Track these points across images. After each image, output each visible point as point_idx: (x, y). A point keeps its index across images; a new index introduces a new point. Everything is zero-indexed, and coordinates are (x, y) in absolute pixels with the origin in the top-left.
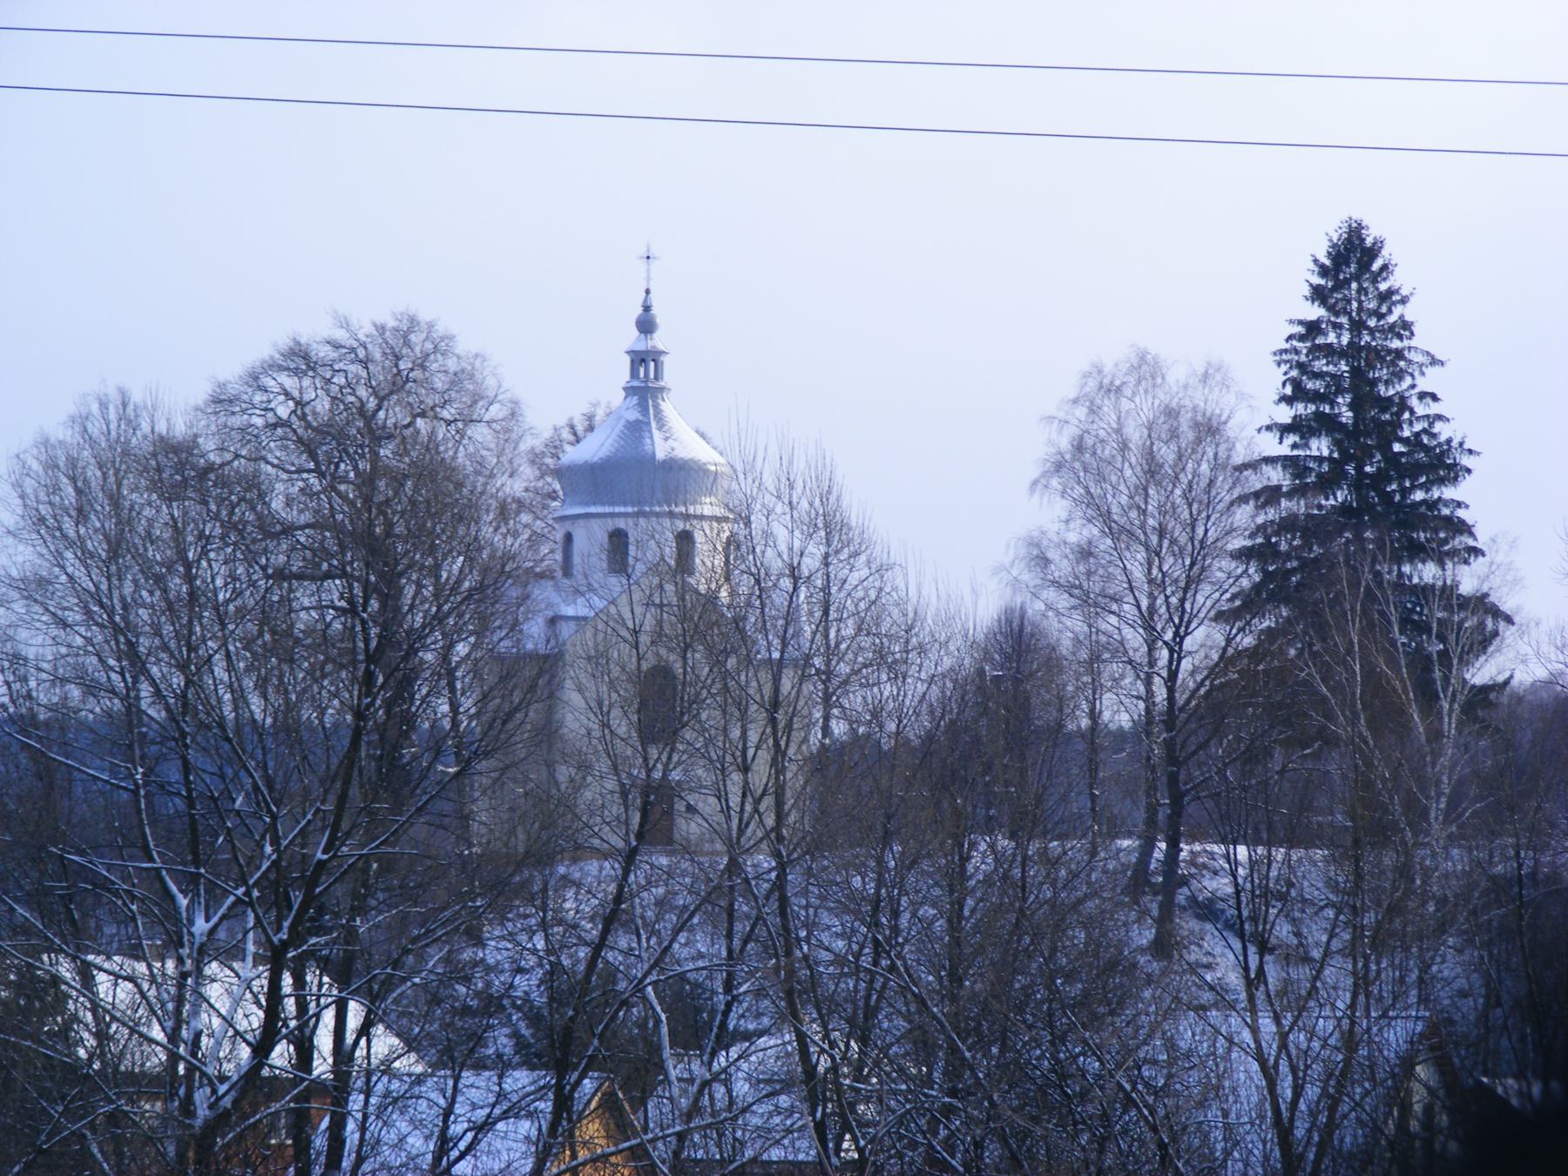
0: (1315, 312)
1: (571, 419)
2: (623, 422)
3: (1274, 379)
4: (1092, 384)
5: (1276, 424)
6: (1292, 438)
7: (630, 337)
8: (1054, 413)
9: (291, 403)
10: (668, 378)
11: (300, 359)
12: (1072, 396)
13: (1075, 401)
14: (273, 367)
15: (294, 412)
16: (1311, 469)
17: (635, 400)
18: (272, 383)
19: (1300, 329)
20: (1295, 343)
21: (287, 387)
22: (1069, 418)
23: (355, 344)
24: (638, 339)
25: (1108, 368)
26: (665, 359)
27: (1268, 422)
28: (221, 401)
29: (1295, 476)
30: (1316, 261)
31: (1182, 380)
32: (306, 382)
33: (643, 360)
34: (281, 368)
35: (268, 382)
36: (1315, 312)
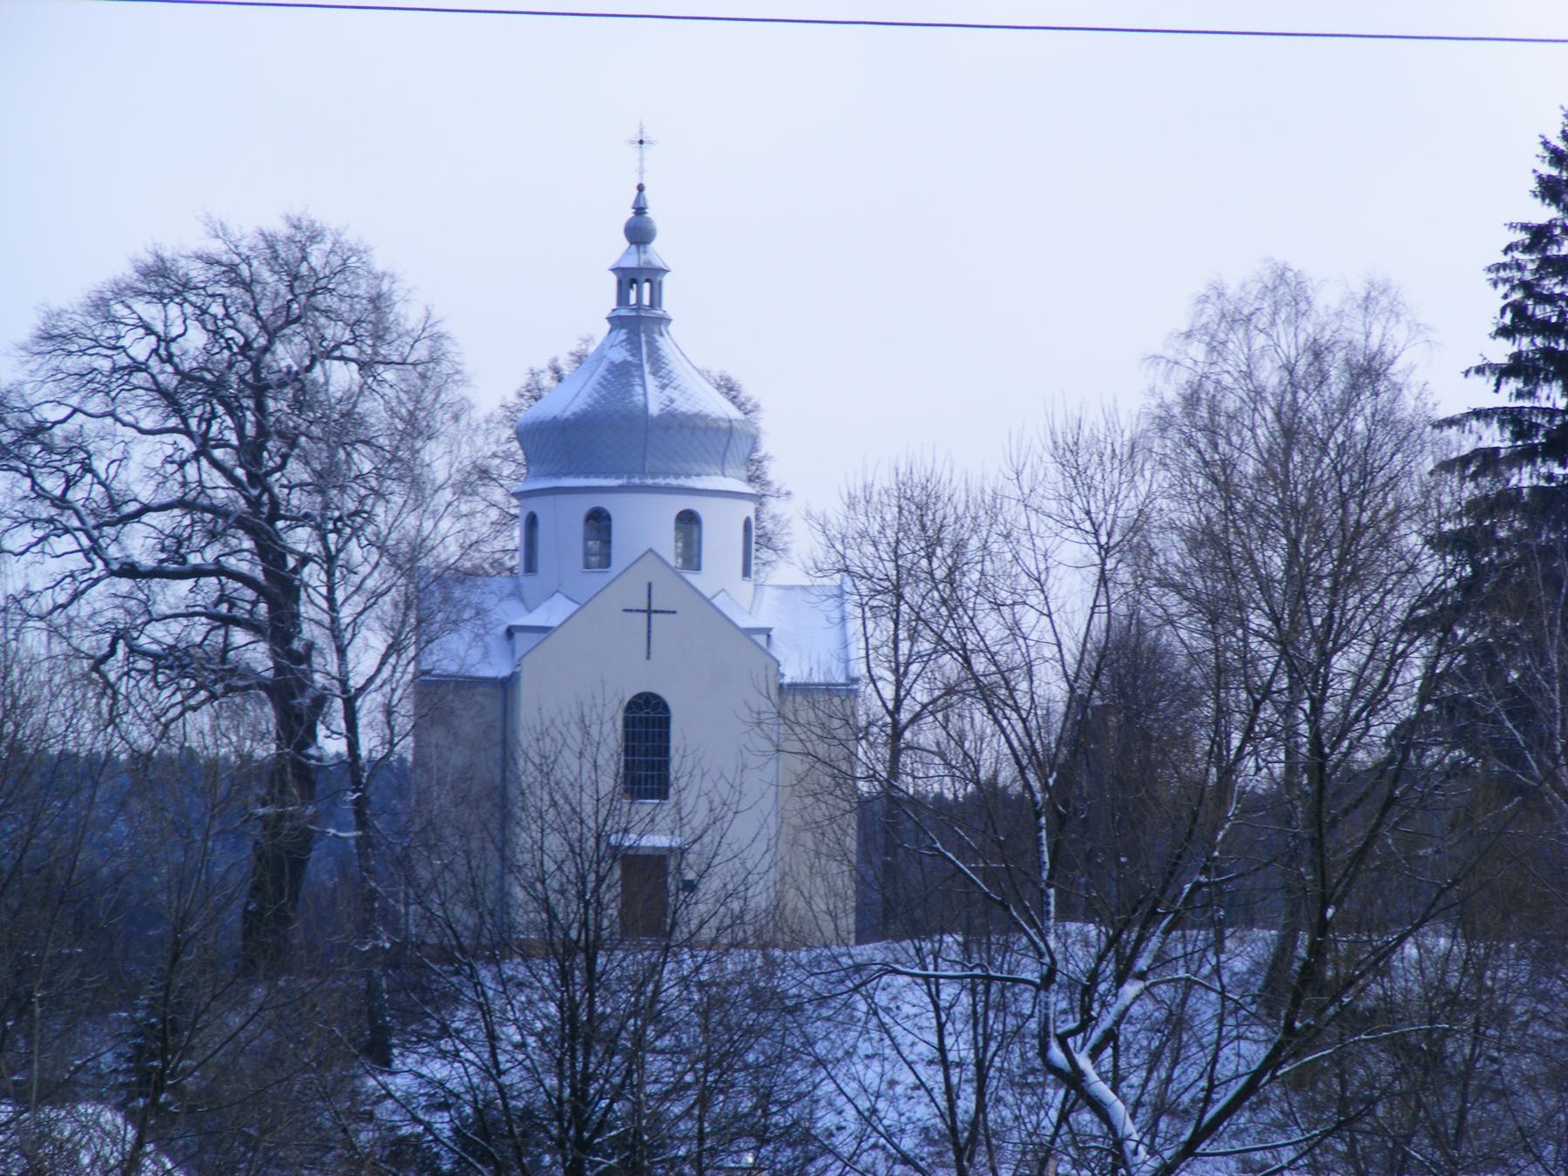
0: (1544, 213)
1: (555, 360)
2: (605, 364)
3: (1491, 303)
4: (1211, 311)
5: (1490, 365)
6: (1514, 384)
7: (617, 248)
8: (1160, 351)
9: (153, 339)
10: (670, 303)
11: (162, 280)
12: (1184, 328)
13: (1188, 335)
14: (122, 292)
15: (155, 351)
16: (1538, 426)
17: (622, 334)
18: (126, 312)
19: (1524, 237)
20: (1517, 255)
21: (146, 318)
22: (1180, 357)
23: (237, 260)
24: (627, 252)
25: (1232, 289)
26: (667, 281)
27: (1479, 362)
28: (51, 338)
29: (1516, 435)
30: (1545, 144)
31: (1335, 305)
32: (174, 311)
33: (634, 281)
34: (139, 293)
35: (119, 310)
36: (1544, 213)
